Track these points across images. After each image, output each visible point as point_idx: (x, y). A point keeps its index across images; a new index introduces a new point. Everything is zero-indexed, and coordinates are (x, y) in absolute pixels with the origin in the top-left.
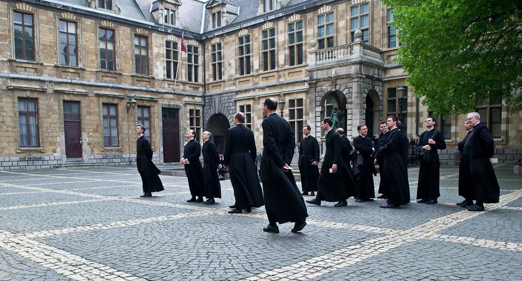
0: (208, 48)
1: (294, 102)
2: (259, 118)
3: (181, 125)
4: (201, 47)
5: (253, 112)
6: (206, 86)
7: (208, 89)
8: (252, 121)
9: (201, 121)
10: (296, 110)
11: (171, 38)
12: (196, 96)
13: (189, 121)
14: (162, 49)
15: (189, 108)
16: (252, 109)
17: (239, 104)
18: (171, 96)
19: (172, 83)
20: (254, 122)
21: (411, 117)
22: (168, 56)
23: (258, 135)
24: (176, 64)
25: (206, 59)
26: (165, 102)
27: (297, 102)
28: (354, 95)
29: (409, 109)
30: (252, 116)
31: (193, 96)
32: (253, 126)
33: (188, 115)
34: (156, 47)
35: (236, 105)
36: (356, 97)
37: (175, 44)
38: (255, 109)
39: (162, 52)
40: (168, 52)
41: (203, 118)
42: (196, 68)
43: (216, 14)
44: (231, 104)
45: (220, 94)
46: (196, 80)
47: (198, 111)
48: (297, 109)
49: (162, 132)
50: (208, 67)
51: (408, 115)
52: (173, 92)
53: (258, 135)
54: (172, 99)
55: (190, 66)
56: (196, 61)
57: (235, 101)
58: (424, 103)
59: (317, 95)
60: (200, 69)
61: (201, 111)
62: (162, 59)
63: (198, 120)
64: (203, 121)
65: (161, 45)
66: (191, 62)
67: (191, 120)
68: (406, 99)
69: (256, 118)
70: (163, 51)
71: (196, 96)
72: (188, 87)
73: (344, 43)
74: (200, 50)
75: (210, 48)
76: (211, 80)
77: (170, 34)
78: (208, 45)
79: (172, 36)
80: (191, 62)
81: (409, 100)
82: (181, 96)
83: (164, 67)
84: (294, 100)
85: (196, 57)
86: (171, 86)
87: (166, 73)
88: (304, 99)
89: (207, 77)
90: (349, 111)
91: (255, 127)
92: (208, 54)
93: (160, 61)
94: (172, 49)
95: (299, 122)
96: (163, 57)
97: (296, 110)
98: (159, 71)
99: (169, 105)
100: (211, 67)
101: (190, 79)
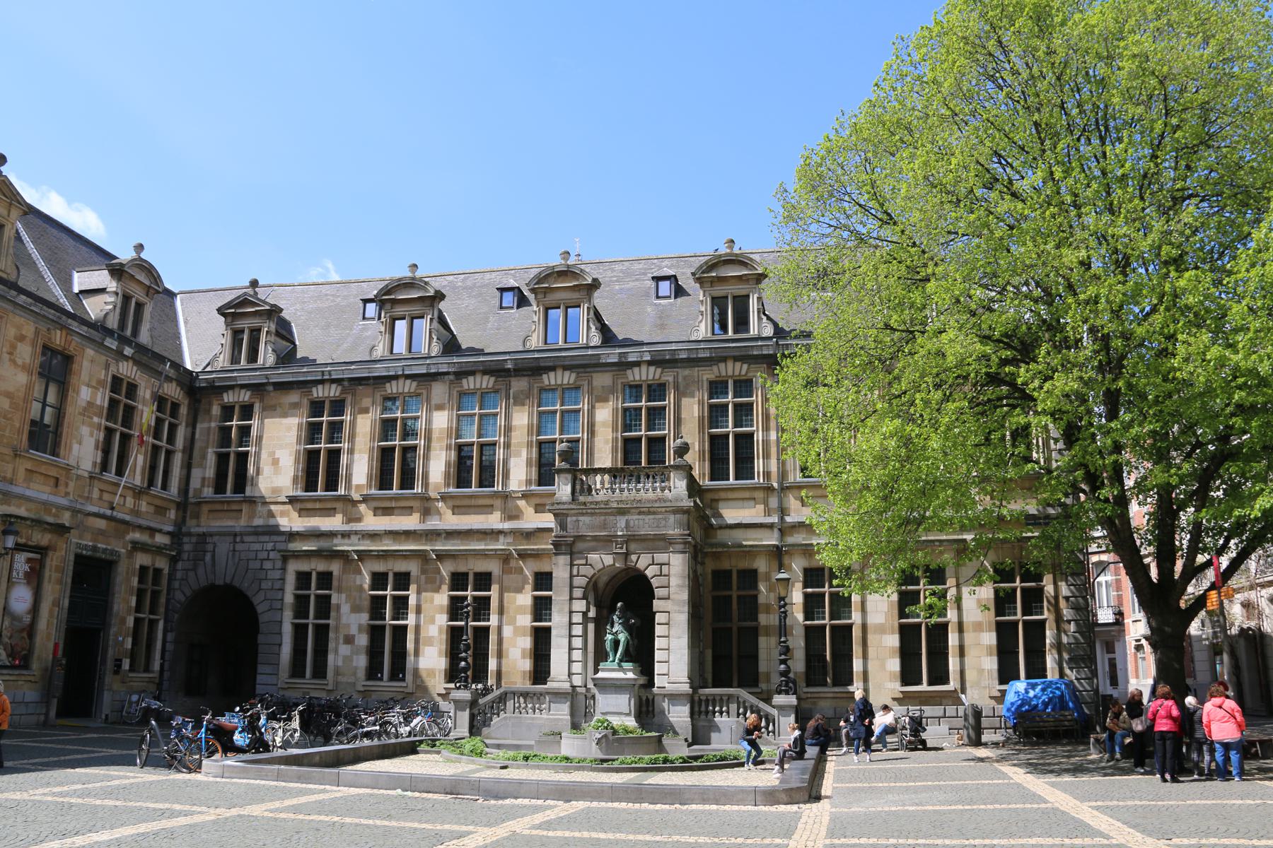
0: (208, 411)
1: (310, 579)
2: (356, 609)
3: (116, 607)
4: (186, 402)
5: (340, 591)
6: (190, 509)
7: (197, 516)
8: (333, 614)
9: (163, 600)
10: (312, 598)
11: (127, 370)
12: (160, 531)
13: (134, 599)
14: (99, 395)
15: (142, 559)
16: (335, 583)
17: (293, 567)
18: (102, 524)
19: (110, 488)
20: (338, 618)
21: (767, 635)
22: (111, 415)
23: (348, 653)
24: (125, 438)
25: (197, 436)
26: (81, 541)
27: (318, 579)
28: (674, 581)
29: (763, 619)
30: (334, 600)
31: (153, 531)
32: (337, 629)
33: (135, 581)
34: (88, 386)
35: (284, 569)
36: (679, 586)
37: (132, 389)
38: (344, 584)
39: (98, 402)
40: (113, 403)
41: (168, 594)
42: (169, 454)
43: (247, 332)
44: (268, 565)
45: (235, 535)
46: (165, 486)
47: (158, 572)
48: (317, 596)
49: (64, 626)
50: (204, 457)
51: (761, 631)
52: (109, 512)
53: (348, 653)
54: (101, 532)
55: (156, 449)
56: (171, 439)
57: (285, 559)
58: (768, 609)
59: (575, 572)
60: (178, 460)
61: (166, 571)
62: (96, 419)
63: (155, 595)
64: (168, 601)
65: (101, 383)
66: (161, 440)
67: (140, 594)
68: (756, 597)
69: (345, 608)
70: (102, 399)
71: (160, 531)
72: (144, 503)
73: (607, 464)
74: (183, 410)
75: (216, 410)
76: (208, 492)
77: (127, 358)
78: (210, 404)
79: (131, 363)
80: (161, 440)
81: (762, 600)
82: (123, 527)
83: (97, 442)
84: (466, 574)
85: (173, 428)
86: (106, 497)
87: (99, 460)
88: (335, 573)
89: (195, 483)
90: (659, 618)
91: (343, 632)
92: (205, 425)
93: (91, 425)
94: (122, 398)
95: (317, 627)
96: (100, 416)
97: (312, 598)
98: (83, 449)
99: (95, 548)
100: (211, 459)
101: (151, 482)
